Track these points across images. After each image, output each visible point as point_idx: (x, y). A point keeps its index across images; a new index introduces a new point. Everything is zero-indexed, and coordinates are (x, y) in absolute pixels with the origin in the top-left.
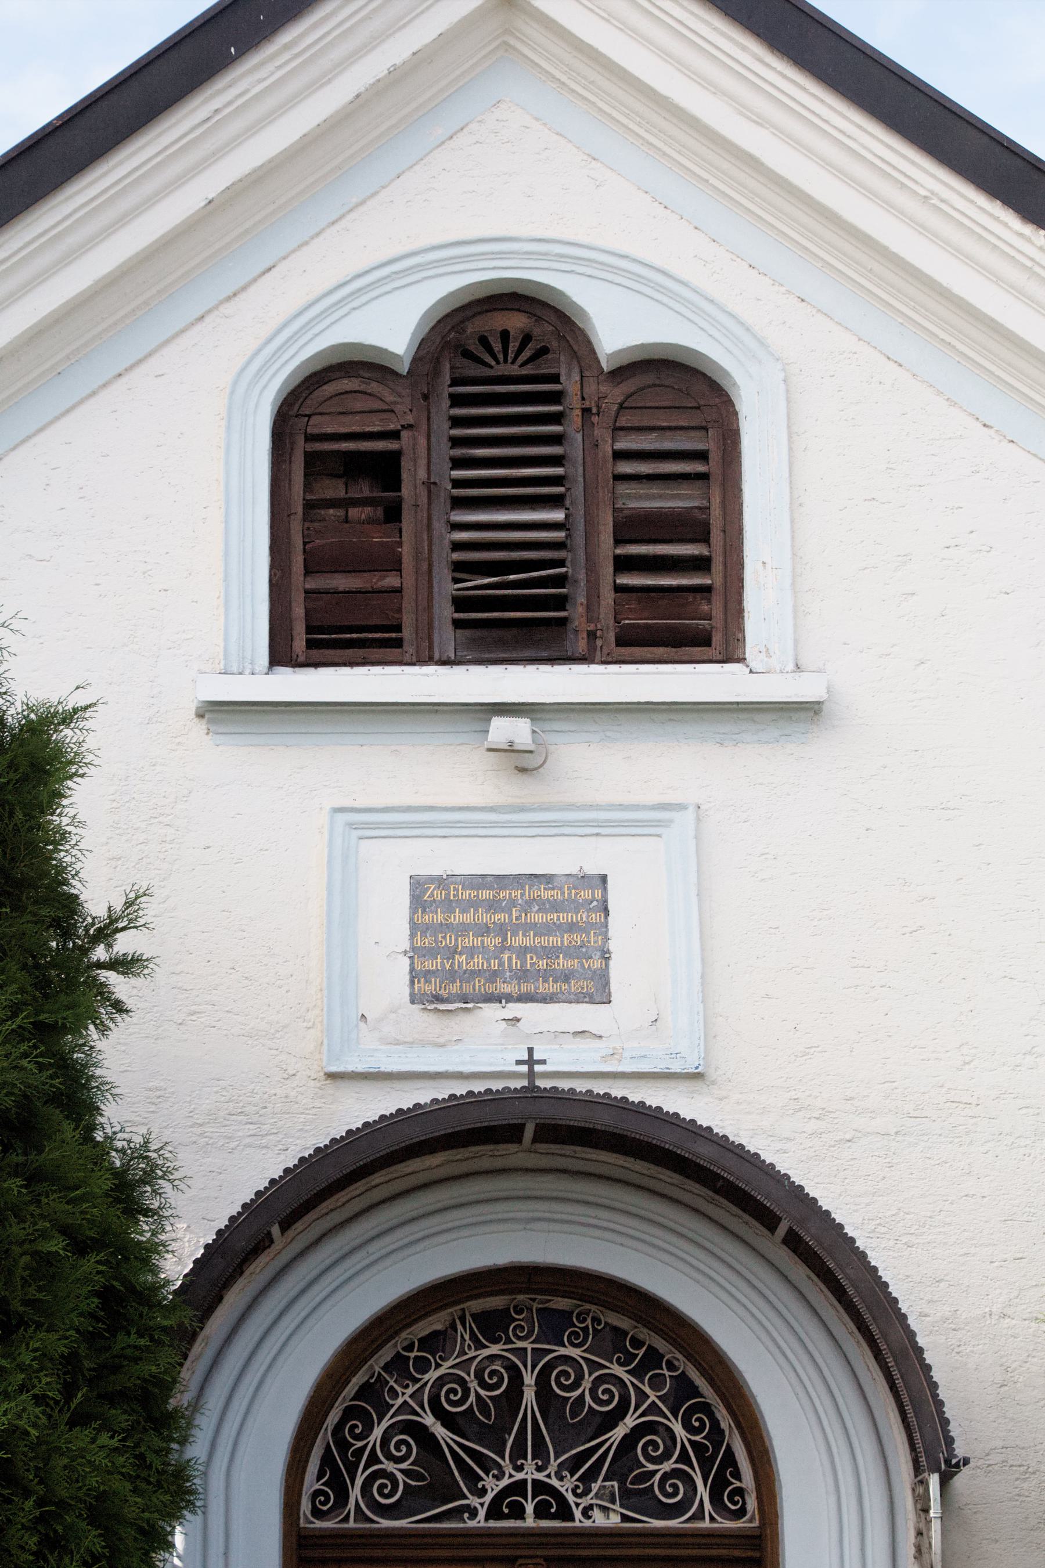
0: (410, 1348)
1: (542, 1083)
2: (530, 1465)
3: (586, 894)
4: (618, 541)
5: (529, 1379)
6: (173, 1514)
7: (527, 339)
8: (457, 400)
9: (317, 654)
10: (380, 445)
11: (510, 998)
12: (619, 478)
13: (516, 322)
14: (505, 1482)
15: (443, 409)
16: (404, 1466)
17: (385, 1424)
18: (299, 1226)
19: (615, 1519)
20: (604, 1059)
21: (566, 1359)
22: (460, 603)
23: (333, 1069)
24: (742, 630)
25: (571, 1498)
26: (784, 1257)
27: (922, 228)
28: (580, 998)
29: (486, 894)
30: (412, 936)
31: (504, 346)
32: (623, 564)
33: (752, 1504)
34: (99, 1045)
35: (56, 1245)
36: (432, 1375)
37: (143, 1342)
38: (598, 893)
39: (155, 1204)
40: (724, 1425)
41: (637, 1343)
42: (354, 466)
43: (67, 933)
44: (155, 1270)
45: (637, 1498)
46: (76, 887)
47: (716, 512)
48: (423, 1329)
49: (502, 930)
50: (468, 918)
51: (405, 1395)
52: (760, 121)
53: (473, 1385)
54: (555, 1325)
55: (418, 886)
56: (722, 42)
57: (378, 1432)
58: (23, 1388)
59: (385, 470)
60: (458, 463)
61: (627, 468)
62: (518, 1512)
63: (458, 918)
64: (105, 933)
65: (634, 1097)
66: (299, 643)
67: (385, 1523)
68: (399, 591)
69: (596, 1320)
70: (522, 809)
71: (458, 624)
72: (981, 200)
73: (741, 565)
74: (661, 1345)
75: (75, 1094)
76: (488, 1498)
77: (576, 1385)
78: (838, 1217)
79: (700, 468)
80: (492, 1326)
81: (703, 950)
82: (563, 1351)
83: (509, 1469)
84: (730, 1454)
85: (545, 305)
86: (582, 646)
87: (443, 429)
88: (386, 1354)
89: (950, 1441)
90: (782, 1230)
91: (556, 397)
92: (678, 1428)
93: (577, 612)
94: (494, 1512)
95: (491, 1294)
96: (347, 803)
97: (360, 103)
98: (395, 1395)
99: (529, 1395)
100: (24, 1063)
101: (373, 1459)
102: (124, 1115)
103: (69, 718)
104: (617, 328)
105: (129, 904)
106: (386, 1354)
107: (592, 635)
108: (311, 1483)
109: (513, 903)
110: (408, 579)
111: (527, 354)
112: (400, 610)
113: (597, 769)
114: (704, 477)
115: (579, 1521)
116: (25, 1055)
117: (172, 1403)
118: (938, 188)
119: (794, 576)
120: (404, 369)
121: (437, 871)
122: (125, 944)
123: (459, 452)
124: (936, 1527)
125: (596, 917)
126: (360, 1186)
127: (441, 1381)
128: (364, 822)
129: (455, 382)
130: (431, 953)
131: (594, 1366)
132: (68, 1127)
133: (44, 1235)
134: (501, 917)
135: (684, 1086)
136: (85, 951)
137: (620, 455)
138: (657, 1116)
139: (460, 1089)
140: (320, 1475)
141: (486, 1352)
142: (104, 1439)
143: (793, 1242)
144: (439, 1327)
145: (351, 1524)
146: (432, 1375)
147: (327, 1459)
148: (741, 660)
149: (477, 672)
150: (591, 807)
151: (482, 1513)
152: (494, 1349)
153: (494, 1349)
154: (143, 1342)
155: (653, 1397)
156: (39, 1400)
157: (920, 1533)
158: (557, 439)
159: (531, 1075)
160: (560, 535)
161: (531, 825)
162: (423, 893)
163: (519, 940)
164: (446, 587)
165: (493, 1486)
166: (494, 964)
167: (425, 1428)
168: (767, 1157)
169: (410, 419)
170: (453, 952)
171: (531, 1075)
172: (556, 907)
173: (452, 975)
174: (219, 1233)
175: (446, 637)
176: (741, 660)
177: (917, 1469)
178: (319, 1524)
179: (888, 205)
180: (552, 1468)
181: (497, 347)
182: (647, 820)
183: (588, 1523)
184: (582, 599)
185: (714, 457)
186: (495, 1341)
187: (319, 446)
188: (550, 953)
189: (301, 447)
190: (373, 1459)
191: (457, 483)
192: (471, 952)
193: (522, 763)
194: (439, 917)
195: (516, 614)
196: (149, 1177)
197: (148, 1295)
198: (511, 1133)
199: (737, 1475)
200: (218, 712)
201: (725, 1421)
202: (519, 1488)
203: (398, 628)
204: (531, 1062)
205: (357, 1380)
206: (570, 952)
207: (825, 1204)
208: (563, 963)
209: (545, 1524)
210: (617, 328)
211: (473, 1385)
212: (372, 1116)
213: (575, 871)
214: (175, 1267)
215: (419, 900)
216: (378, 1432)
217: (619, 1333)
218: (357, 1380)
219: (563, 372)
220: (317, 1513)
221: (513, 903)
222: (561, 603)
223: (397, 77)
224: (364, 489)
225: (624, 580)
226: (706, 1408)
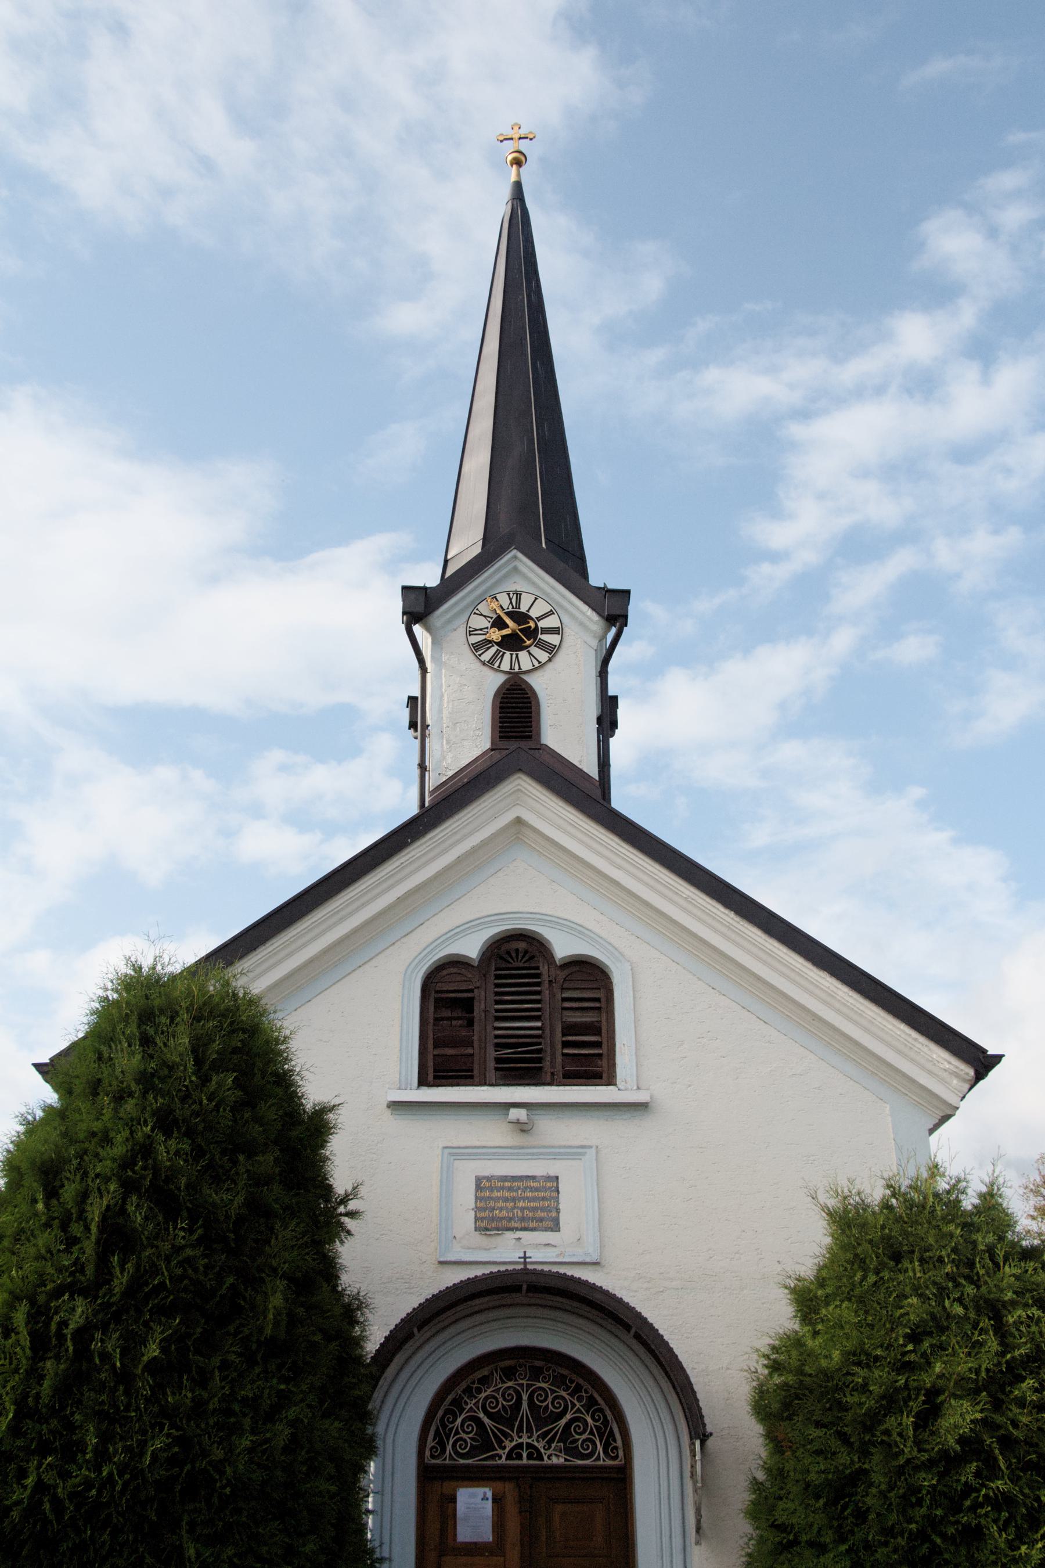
0: (473, 1383)
1: (529, 1267)
2: (525, 1435)
3: (549, 1184)
4: (564, 1035)
5: (525, 1397)
6: (369, 1458)
7: (526, 952)
8: (497, 977)
9: (438, 1081)
10: (465, 995)
11: (517, 1229)
12: (564, 1009)
13: (522, 945)
14: (514, 1443)
15: (492, 980)
16: (471, 1435)
17: (463, 1416)
18: (426, 1328)
19: (562, 1460)
20: (558, 1256)
21: (541, 1388)
22: (498, 1060)
23: (442, 1259)
24: (615, 1072)
25: (542, 1451)
26: (634, 1344)
27: (684, 910)
28: (546, 1229)
29: (507, 1184)
30: (476, 1202)
31: (516, 954)
32: (566, 1044)
33: (621, 1453)
34: (340, 1249)
35: (318, 1338)
36: (483, 1395)
37: (354, 1380)
38: (555, 1184)
39: (362, 1320)
40: (609, 1418)
41: (572, 1381)
42: (454, 1003)
43: (327, 1201)
44: (362, 1347)
45: (572, 1451)
46: (331, 1181)
47: (604, 1023)
48: (479, 1375)
49: (514, 1200)
50: (499, 1194)
51: (471, 1404)
52: (619, 868)
53: (501, 1400)
54: (536, 1374)
55: (479, 1180)
56: (603, 837)
57: (459, 1420)
58: (302, 1401)
59: (467, 1005)
60: (497, 1002)
61: (567, 1005)
62: (519, 1457)
63: (495, 1194)
64: (344, 1201)
65: (569, 1273)
66: (431, 1077)
67: (462, 1461)
68: (472, 1055)
69: (554, 1371)
70: (523, 1148)
71: (496, 1069)
72: (708, 899)
73: (614, 1045)
74: (581, 1382)
75: (329, 1270)
76: (507, 1451)
77: (465, 1441)
78: (656, 1326)
79: (598, 1005)
80: (509, 1373)
81: (599, 1209)
82: (539, 1385)
83: (516, 1438)
84: (611, 1432)
85: (534, 939)
86: (548, 1079)
87: (491, 988)
88: (464, 1385)
89: (704, 1425)
90: (633, 1331)
91: (538, 976)
92: (589, 1420)
93: (546, 1064)
94: (509, 1457)
95: (510, 1359)
96: (450, 1144)
97: (459, 860)
98: (466, 1403)
99: (525, 1405)
100: (307, 1257)
101: (457, 1433)
102: (350, 1280)
103: (332, 1109)
104: (563, 947)
105: (354, 1188)
106: (464, 1385)
107: (553, 1074)
108: (430, 1443)
109: (519, 1188)
110: (475, 1050)
111: (526, 958)
112: (472, 1063)
113: (555, 1131)
114: (599, 1009)
115: (546, 1461)
116: (308, 1254)
117: (370, 1407)
118: (691, 894)
119: (637, 1049)
120: (476, 964)
121: (486, 1174)
122: (352, 1205)
123: (498, 998)
124: (699, 1463)
125: (554, 1194)
126: (453, 1311)
127: (486, 1398)
128: (456, 1153)
129: (497, 969)
130: (484, 1209)
131: (553, 1392)
132: (325, 1285)
133: (314, 1334)
134: (514, 1194)
135: (590, 1268)
136: (336, 1209)
137: (564, 1000)
138: (579, 1281)
139: (495, 1269)
140: (434, 1440)
141: (506, 1385)
142: (336, 1424)
143: (637, 1337)
144: (486, 1373)
145: (447, 1462)
146: (483, 1395)
147: (437, 1433)
148: (615, 1085)
149: (504, 1089)
150: (553, 1147)
151: (504, 1457)
152: (510, 1384)
153: (510, 1384)
154: (354, 1380)
155: (578, 1405)
156: (309, 1406)
157: (692, 1466)
158: (538, 993)
159: (525, 1263)
160: (539, 1032)
161: (528, 1154)
162: (481, 1183)
163: (521, 1204)
164: (492, 1053)
165: (509, 1445)
166: (511, 1215)
167: (479, 1419)
168: (626, 1299)
169: (478, 984)
170: (493, 1209)
171: (525, 1263)
172: (537, 1190)
173: (493, 1219)
174: (391, 1332)
175: (492, 1074)
176: (615, 1085)
177: (691, 1438)
178: (433, 1461)
179: (671, 901)
180: (535, 1437)
181: (514, 955)
182: (576, 1152)
183: (550, 1462)
184: (548, 1059)
185: (603, 1000)
186: (510, 1380)
187: (439, 995)
188: (534, 1209)
189: (433, 995)
190: (457, 1433)
191: (497, 1011)
192: (501, 1209)
193: (523, 1128)
194: (487, 1194)
195: (522, 1068)
196: (359, 1308)
197: (359, 1360)
198: (517, 1289)
199: (615, 1440)
200: (396, 1106)
201: (610, 1417)
202: (520, 1446)
203: (472, 1071)
204: (525, 1257)
205: (450, 1398)
206: (543, 1209)
207: (650, 1320)
208: (540, 1214)
209: (531, 1462)
210: (563, 947)
211: (501, 1400)
212: (457, 1281)
213: (545, 1174)
214: (372, 1345)
215: (479, 1187)
216: (459, 1420)
217: (564, 1377)
218: (450, 1398)
219: (541, 965)
220: (433, 1457)
221: (519, 1188)
222: (539, 1060)
223: (474, 850)
224: (458, 1013)
225: (566, 1051)
226: (601, 1410)
